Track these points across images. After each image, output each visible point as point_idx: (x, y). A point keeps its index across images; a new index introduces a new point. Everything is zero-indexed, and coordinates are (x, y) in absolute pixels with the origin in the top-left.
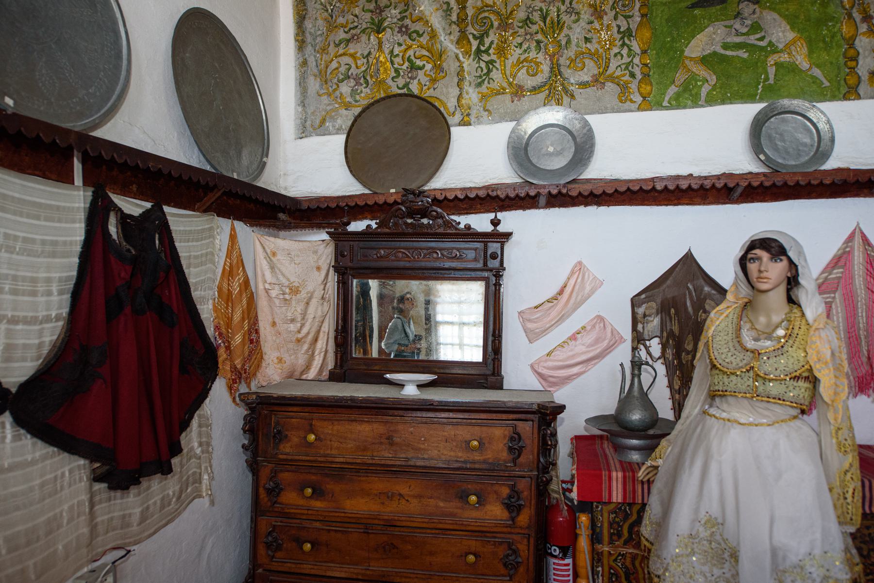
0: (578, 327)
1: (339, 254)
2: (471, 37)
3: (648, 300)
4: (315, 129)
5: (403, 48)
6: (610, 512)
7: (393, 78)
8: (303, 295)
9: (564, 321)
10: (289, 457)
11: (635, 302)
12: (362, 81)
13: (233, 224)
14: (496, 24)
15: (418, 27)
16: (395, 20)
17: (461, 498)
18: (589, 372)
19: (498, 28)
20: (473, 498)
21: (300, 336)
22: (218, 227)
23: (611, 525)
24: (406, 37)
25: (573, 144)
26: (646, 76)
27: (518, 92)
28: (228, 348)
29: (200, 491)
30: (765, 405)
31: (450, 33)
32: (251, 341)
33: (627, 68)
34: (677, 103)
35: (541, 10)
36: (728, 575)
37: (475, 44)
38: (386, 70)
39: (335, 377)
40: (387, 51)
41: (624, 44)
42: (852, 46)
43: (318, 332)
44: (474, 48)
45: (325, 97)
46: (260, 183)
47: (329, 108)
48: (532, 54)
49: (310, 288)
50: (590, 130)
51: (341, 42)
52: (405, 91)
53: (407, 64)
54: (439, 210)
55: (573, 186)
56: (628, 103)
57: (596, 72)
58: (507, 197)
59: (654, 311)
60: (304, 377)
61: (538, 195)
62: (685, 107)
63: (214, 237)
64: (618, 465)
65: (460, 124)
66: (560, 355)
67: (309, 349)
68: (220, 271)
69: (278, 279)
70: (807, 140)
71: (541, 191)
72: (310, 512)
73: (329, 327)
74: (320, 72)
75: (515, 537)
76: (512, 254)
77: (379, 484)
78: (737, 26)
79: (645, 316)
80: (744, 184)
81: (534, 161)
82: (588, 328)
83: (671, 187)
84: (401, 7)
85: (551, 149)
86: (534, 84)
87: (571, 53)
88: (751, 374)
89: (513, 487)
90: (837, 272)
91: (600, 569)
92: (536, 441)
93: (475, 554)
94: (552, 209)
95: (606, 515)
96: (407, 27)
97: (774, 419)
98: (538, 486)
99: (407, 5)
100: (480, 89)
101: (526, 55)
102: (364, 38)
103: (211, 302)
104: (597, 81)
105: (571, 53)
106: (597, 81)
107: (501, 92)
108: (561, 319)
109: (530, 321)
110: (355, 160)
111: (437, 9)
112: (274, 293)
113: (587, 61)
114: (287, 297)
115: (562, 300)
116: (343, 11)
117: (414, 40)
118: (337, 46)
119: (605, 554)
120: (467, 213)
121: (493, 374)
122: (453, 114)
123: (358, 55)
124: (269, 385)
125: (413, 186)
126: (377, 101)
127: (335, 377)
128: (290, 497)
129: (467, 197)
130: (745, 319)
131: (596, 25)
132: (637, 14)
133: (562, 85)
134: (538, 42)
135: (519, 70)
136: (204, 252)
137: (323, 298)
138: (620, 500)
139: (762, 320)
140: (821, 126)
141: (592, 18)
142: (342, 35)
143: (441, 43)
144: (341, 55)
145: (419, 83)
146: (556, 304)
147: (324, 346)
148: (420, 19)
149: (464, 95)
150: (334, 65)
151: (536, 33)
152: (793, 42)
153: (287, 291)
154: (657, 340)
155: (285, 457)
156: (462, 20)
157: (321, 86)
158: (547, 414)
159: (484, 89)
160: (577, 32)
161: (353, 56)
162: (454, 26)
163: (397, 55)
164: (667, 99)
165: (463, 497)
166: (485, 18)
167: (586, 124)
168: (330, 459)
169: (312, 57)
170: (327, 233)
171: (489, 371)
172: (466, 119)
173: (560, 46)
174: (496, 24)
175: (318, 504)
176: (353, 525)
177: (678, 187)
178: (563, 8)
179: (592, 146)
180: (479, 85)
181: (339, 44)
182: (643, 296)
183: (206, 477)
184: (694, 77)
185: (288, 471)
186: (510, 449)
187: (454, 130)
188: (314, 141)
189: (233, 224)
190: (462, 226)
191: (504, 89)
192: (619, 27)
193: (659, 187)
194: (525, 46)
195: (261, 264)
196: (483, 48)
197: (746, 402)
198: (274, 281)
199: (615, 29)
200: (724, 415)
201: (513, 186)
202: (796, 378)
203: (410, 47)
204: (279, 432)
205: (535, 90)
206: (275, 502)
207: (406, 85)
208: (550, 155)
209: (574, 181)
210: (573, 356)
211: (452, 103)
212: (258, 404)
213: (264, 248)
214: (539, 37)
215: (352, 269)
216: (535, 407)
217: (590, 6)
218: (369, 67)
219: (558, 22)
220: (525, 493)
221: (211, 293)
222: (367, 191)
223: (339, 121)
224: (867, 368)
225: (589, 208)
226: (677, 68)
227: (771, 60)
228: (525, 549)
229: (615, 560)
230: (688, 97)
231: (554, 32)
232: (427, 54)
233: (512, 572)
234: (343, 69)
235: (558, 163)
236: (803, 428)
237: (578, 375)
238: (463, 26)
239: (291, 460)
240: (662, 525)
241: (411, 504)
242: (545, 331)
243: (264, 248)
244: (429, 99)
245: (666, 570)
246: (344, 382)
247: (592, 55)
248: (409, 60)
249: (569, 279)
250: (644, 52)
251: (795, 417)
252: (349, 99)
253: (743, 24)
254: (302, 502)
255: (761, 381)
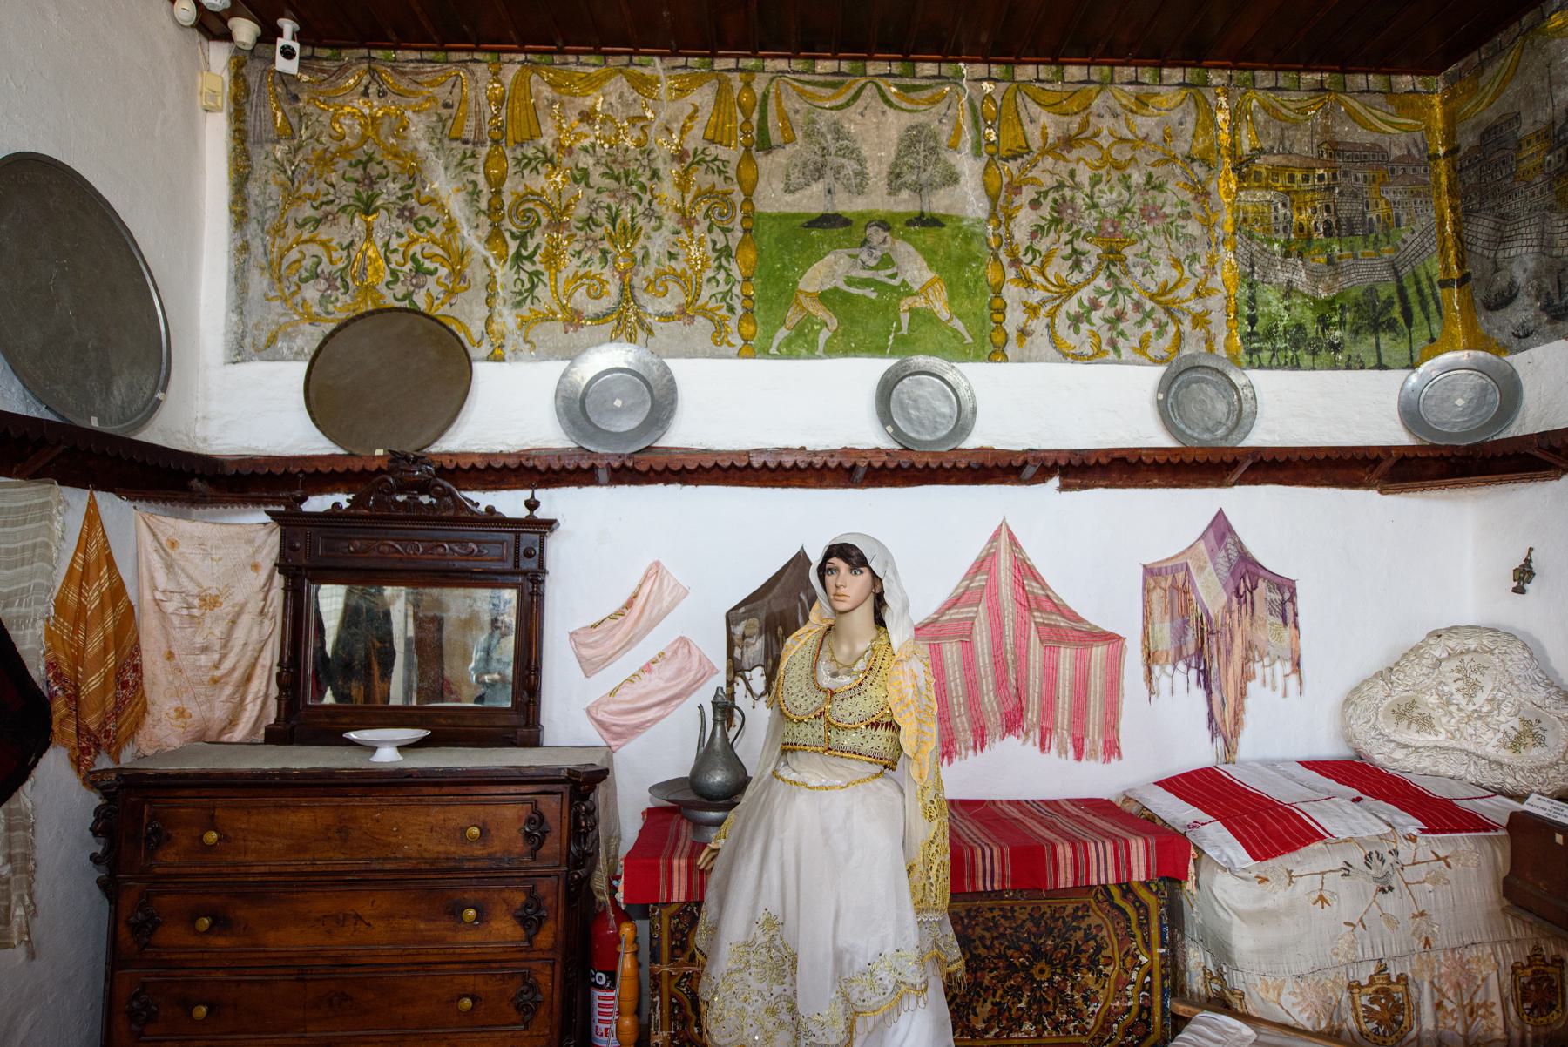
0: (653, 654)
1: (286, 546)
2: (507, 235)
3: (749, 615)
4: (258, 350)
5: (405, 240)
6: (671, 917)
7: (387, 284)
8: (226, 608)
9: (634, 645)
10: (173, 870)
11: (731, 619)
12: (339, 283)
13: (92, 498)
14: (545, 220)
15: (429, 212)
16: (394, 198)
17: (452, 913)
18: (667, 719)
19: (547, 227)
20: (471, 912)
21: (218, 673)
22: (60, 503)
23: (672, 935)
24: (411, 226)
25: (648, 397)
26: (749, 311)
27: (574, 319)
28: (74, 698)
29: (8, 937)
30: (837, 761)
31: (477, 227)
32: (125, 685)
33: (724, 299)
34: (788, 351)
35: (609, 208)
36: (789, 993)
37: (513, 246)
38: (376, 270)
39: (276, 736)
40: (380, 243)
41: (720, 267)
42: (998, 295)
43: (253, 666)
44: (512, 251)
45: (278, 302)
46: (151, 435)
47: (282, 320)
48: (596, 268)
49: (239, 597)
50: (672, 380)
51: (306, 222)
52: (405, 304)
53: (410, 265)
54: (447, 484)
55: (644, 456)
56: (725, 346)
57: (683, 300)
58: (549, 469)
59: (756, 630)
60: (225, 738)
61: (593, 468)
62: (798, 357)
63: (51, 520)
64: (687, 850)
65: (488, 359)
66: (628, 693)
67: (234, 693)
68: (63, 571)
69: (178, 583)
70: (945, 410)
71: (598, 462)
72: (206, 956)
73: (270, 658)
74: (271, 264)
75: (534, 965)
76: (558, 552)
77: (323, 904)
78: (864, 256)
79: (744, 637)
80: (863, 464)
81: (594, 419)
82: (668, 654)
83: (772, 465)
84: (404, 180)
85: (618, 403)
86: (598, 310)
87: (649, 271)
88: (822, 720)
89: (530, 893)
90: (981, 579)
91: (657, 999)
92: (566, 822)
93: (473, 998)
94: (619, 488)
95: (665, 920)
96: (411, 210)
97: (850, 779)
98: (567, 887)
99: (412, 178)
100: (519, 311)
101: (587, 268)
102: (343, 219)
103: (41, 623)
104: (684, 313)
105: (649, 271)
106: (683, 312)
107: (549, 317)
108: (629, 643)
109: (585, 645)
110: (321, 401)
111: (459, 190)
112: (170, 607)
113: (671, 285)
114: (196, 612)
115: (630, 614)
116: (311, 176)
117: (422, 231)
118: (300, 226)
119: (665, 976)
120: (496, 489)
121: (527, 725)
122: (479, 344)
123: (334, 244)
124: (161, 754)
125: (409, 448)
126: (362, 316)
127: (276, 736)
128: (172, 936)
129: (489, 467)
130: (825, 647)
131: (684, 237)
132: (738, 227)
133: (636, 314)
134: (604, 253)
135: (576, 289)
136: (29, 542)
137: (262, 612)
138: (682, 899)
139: (845, 649)
140: (962, 393)
141: (679, 227)
142: (307, 211)
143: (463, 239)
144: (306, 242)
145: (429, 294)
146: (623, 622)
147: (263, 689)
148: (432, 201)
149: (496, 317)
150: (294, 255)
151: (602, 239)
152: (931, 283)
153: (196, 602)
154: (759, 670)
155: (166, 870)
156: (494, 210)
157: (271, 285)
158: (584, 784)
159: (525, 310)
160: (658, 244)
161: (325, 245)
162: (482, 217)
163: (395, 251)
164: (775, 344)
165: (455, 912)
166: (529, 210)
167: (667, 371)
168: (243, 869)
169: (258, 242)
170: (268, 513)
171: (522, 722)
172: (498, 352)
173: (634, 261)
174: (545, 220)
175: (221, 942)
176: (279, 971)
177: (780, 464)
178: (640, 209)
179: (674, 401)
180: (519, 304)
181: (303, 225)
182: (742, 610)
183: (19, 912)
184: (810, 318)
185: (171, 893)
186: (528, 836)
187: (482, 370)
188: (257, 369)
189: (92, 498)
190: (482, 508)
191: (554, 314)
192: (714, 243)
193: (756, 463)
194: (585, 256)
195: (148, 561)
196: (524, 253)
197: (817, 757)
198: (172, 586)
199: (710, 246)
200: (794, 776)
201: (559, 454)
202: (875, 725)
203: (415, 241)
204: (156, 831)
205: (598, 318)
206: (147, 945)
207: (408, 296)
208: (617, 411)
209: (649, 448)
210: (646, 695)
211: (477, 328)
212: (120, 787)
213: (154, 535)
214: (606, 245)
215: (308, 568)
216: (564, 774)
217: (677, 210)
218: (350, 264)
219: (633, 227)
220: (549, 900)
221: (42, 609)
222: (340, 451)
223: (299, 342)
224: (1016, 700)
225: (671, 487)
226: (788, 305)
227: (905, 304)
228: (547, 979)
229: (678, 984)
230: (801, 344)
231: (626, 241)
232: (441, 252)
233: (527, 1017)
234: (308, 263)
235: (626, 424)
236: (884, 787)
237: (655, 720)
238: (496, 217)
239: (177, 875)
240: (715, 929)
241: (378, 928)
242: (607, 660)
243: (154, 535)
244: (447, 321)
245: (715, 993)
246: (291, 743)
247: (679, 277)
248: (414, 259)
249: (640, 586)
250: (747, 279)
251: (877, 776)
252: (316, 309)
253: (871, 255)
254: (193, 941)
255: (834, 731)
